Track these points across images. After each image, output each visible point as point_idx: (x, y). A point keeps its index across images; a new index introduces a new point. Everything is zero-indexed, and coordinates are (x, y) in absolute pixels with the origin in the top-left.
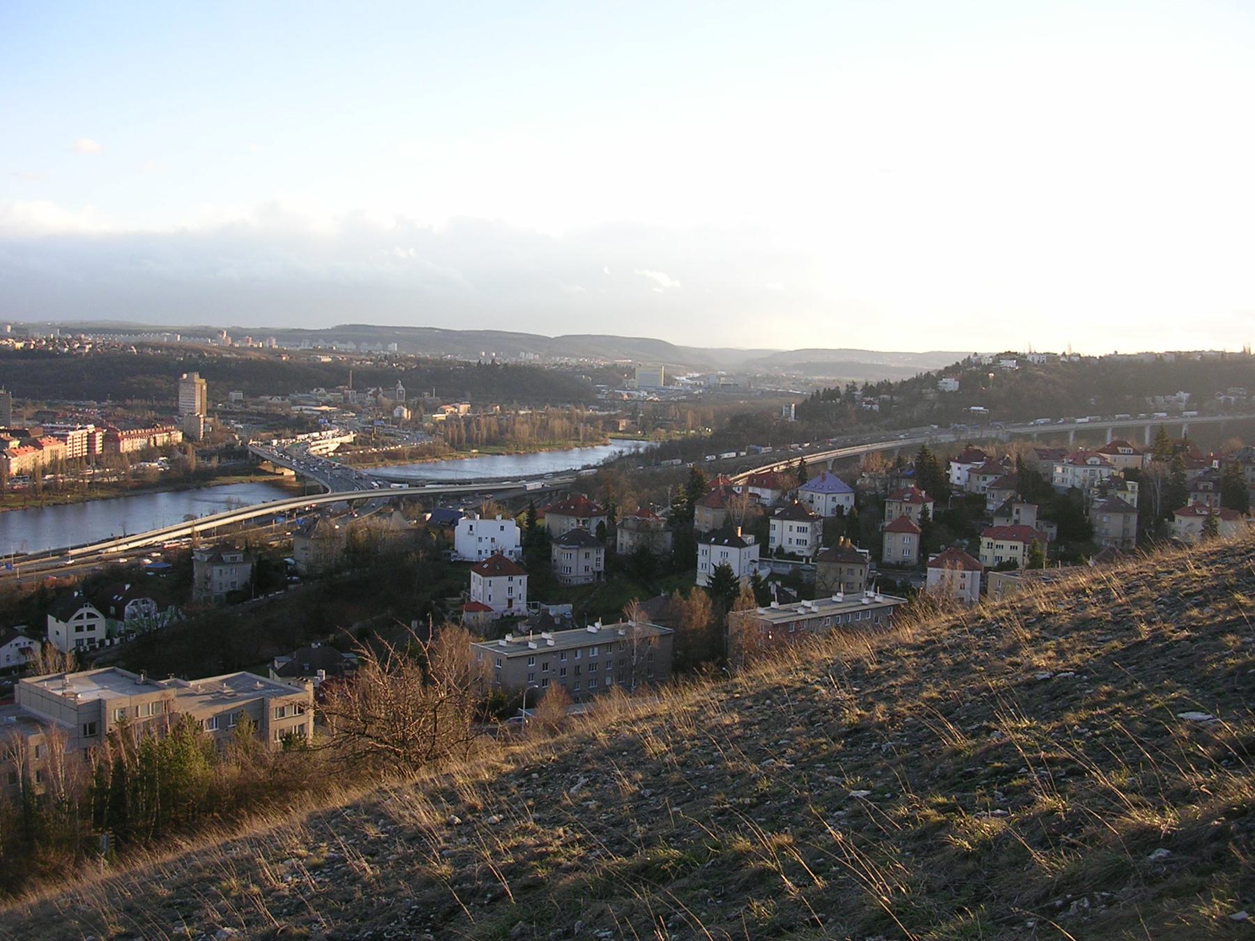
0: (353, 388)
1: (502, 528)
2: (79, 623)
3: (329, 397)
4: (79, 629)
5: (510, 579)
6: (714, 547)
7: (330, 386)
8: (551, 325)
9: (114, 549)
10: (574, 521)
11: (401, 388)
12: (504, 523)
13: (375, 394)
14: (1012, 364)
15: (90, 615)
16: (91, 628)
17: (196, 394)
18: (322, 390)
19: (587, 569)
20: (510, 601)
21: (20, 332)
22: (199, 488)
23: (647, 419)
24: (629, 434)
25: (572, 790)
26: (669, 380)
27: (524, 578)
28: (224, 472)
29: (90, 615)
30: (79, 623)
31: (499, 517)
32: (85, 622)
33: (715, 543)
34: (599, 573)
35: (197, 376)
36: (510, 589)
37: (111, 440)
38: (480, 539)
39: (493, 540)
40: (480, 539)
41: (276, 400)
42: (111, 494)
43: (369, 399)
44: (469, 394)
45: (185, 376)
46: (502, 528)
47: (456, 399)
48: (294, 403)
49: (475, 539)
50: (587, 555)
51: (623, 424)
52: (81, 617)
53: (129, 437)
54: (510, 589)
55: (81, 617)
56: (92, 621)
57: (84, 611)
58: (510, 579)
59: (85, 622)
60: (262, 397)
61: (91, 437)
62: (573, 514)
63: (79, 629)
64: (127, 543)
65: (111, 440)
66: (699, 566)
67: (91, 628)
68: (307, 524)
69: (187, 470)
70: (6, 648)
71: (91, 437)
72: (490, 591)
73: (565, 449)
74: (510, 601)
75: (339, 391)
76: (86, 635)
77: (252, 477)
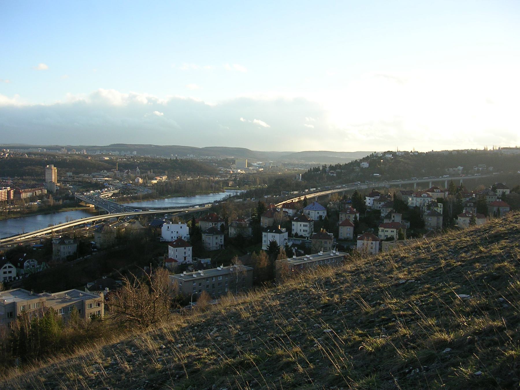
0: (118, 170)
1: (181, 227)
2: (5, 270)
3: (108, 174)
5: (185, 248)
6: (269, 234)
7: (109, 170)
8: (200, 145)
9: (19, 239)
10: (211, 224)
11: (138, 170)
12: (182, 225)
13: (128, 173)
15: (10, 267)
16: (10, 272)
17: (53, 174)
18: (105, 171)
19: (216, 243)
20: (185, 258)
22: (54, 213)
23: (241, 181)
24: (233, 187)
27: (191, 248)
29: (10, 267)
30: (5, 270)
31: (180, 223)
32: (8, 270)
33: (269, 232)
34: (222, 245)
35: (53, 166)
36: (185, 253)
37: (17, 193)
38: (172, 232)
39: (177, 232)
40: (172, 232)
41: (86, 176)
42: (19, 215)
43: (125, 175)
44: (166, 172)
45: (48, 166)
46: (181, 227)
47: (161, 174)
48: (94, 177)
49: (170, 232)
50: (217, 238)
51: (231, 183)
52: (5, 268)
53: (25, 192)
54: (185, 253)
55: (5, 268)
56: (10, 269)
57: (7, 265)
59: (8, 270)
60: (80, 175)
61: (9, 192)
62: (211, 221)
63: (5, 273)
64: (24, 236)
65: (17, 193)
66: (263, 241)
67: (10, 272)
68: (100, 227)
69: (49, 206)
71: (9, 192)
72: (177, 253)
73: (207, 194)
74: (185, 258)
75: (112, 171)
77: (77, 208)
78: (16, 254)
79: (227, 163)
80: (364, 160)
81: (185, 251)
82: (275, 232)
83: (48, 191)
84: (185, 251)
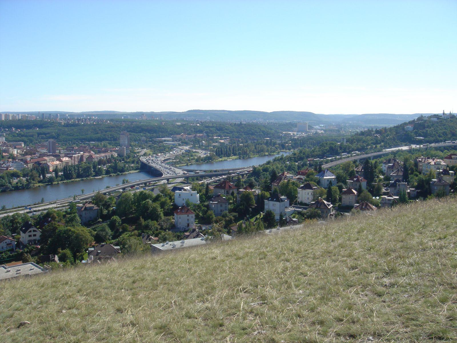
2: (30, 234)
4: (30, 236)
5: (188, 216)
14: (435, 119)
15: (34, 231)
16: (35, 235)
21: (7, 115)
23: (296, 143)
25: (232, 276)
26: (310, 127)
28: (15, 190)
29: (34, 231)
30: (30, 234)
32: (32, 233)
52: (30, 231)
54: (188, 220)
55: (30, 231)
56: (35, 233)
58: (188, 216)
59: (32, 233)
60: (45, 158)
63: (30, 236)
67: (35, 235)
68: (41, 214)
70: (2, 243)
76: (33, 238)
78: (14, 225)
79: (291, 126)
80: (410, 123)
81: (188, 218)
82: (275, 201)
83: (118, 155)
84: (188, 218)
